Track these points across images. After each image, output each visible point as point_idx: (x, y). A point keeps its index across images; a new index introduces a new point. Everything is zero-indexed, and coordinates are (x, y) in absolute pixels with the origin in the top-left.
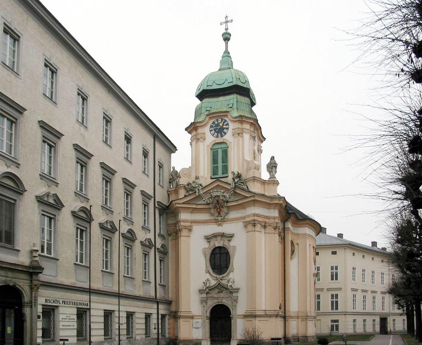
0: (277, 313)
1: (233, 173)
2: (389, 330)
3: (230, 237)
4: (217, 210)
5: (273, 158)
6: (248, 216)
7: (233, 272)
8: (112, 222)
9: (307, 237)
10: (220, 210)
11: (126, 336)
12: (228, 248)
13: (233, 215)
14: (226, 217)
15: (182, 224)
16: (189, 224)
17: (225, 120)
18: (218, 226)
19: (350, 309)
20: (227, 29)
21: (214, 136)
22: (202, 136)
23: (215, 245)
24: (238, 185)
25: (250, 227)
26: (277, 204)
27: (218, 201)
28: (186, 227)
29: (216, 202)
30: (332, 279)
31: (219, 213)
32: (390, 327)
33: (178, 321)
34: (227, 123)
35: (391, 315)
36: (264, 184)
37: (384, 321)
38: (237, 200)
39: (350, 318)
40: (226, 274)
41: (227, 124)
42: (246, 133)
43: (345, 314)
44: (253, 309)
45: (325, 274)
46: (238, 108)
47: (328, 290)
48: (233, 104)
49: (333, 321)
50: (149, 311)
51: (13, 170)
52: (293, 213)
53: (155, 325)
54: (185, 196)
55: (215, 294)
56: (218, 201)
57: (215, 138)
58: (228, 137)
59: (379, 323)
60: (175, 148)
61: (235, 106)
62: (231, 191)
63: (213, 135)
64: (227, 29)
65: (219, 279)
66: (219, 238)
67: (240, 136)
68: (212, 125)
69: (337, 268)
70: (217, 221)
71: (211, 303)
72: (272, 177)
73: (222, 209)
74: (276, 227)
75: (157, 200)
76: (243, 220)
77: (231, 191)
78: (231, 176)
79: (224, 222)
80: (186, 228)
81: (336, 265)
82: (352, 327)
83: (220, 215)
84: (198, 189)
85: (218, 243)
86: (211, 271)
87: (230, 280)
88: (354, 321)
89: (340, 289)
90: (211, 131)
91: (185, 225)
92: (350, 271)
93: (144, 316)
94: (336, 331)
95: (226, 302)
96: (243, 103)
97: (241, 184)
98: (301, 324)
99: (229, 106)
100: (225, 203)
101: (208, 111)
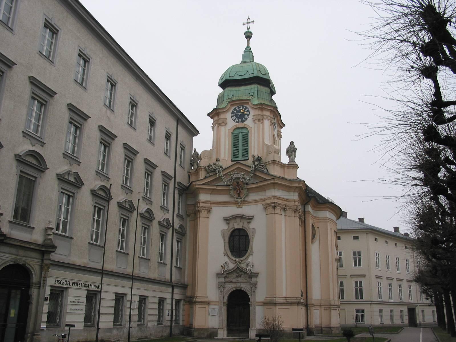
0: (298, 301)
1: (253, 156)
2: (418, 322)
3: (250, 219)
4: (237, 191)
5: (292, 143)
6: (268, 198)
7: (252, 255)
9: (328, 220)
10: (240, 192)
11: (137, 323)
12: (248, 230)
13: (253, 197)
14: (246, 199)
15: (201, 204)
16: (208, 205)
17: (246, 107)
18: (238, 208)
20: (248, 29)
21: (236, 121)
23: (234, 227)
24: (258, 168)
25: (270, 210)
26: (296, 187)
27: (238, 183)
28: (205, 208)
29: (236, 184)
30: (355, 265)
31: (239, 195)
32: (419, 319)
33: (193, 307)
34: (248, 109)
35: (419, 305)
36: (284, 168)
37: (412, 312)
38: (257, 183)
39: (376, 308)
40: (245, 257)
44: (273, 296)
46: (259, 96)
47: (352, 276)
49: (358, 311)
50: (163, 295)
53: (169, 311)
54: (206, 177)
55: (234, 278)
56: (238, 183)
57: (236, 124)
58: (249, 122)
59: (407, 314)
61: (256, 95)
63: (234, 121)
64: (248, 29)
65: (238, 262)
66: (238, 220)
67: (261, 122)
68: (234, 111)
69: (359, 253)
70: (236, 203)
71: (229, 288)
72: (292, 160)
73: (242, 191)
74: (296, 210)
75: (177, 180)
76: (263, 203)
78: (251, 159)
79: (243, 203)
80: (205, 208)
81: (359, 250)
83: (240, 197)
84: (219, 171)
85: (237, 225)
86: (229, 254)
87: (249, 264)
88: (381, 311)
89: (364, 276)
90: (232, 116)
91: (204, 206)
92: (373, 257)
93: (157, 300)
95: (245, 287)
96: (263, 92)
97: (261, 167)
100: (245, 185)
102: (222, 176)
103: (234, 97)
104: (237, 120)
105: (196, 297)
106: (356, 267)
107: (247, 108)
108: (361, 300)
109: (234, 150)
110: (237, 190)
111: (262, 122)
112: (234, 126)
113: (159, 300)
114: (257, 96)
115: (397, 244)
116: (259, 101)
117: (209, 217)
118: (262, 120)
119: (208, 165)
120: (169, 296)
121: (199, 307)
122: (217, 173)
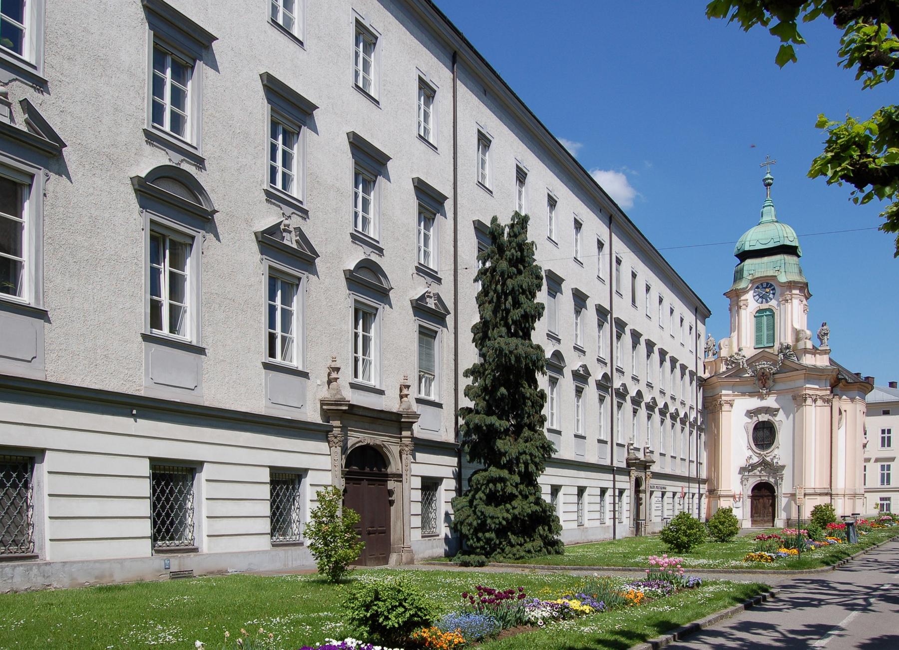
1: (781, 344)
8: (439, 298)
15: (723, 398)
30: (883, 445)
34: (773, 287)
41: (774, 289)
42: (796, 298)
45: (875, 438)
47: (877, 460)
49: (882, 499)
51: (374, 258)
52: (842, 379)
57: (759, 305)
60: (710, 312)
61: (782, 270)
63: (757, 301)
69: (889, 431)
71: (752, 482)
73: (768, 381)
75: (614, 316)
78: (777, 346)
80: (727, 402)
84: (743, 362)
85: (763, 417)
89: (893, 459)
90: (754, 296)
93: (575, 491)
98: (849, 502)
99: (776, 269)
103: (757, 273)
106: (883, 449)
108: (883, 463)
109: (757, 336)
113: (271, 475)
116: (788, 277)
118: (791, 299)
120: (610, 485)
122: (741, 364)
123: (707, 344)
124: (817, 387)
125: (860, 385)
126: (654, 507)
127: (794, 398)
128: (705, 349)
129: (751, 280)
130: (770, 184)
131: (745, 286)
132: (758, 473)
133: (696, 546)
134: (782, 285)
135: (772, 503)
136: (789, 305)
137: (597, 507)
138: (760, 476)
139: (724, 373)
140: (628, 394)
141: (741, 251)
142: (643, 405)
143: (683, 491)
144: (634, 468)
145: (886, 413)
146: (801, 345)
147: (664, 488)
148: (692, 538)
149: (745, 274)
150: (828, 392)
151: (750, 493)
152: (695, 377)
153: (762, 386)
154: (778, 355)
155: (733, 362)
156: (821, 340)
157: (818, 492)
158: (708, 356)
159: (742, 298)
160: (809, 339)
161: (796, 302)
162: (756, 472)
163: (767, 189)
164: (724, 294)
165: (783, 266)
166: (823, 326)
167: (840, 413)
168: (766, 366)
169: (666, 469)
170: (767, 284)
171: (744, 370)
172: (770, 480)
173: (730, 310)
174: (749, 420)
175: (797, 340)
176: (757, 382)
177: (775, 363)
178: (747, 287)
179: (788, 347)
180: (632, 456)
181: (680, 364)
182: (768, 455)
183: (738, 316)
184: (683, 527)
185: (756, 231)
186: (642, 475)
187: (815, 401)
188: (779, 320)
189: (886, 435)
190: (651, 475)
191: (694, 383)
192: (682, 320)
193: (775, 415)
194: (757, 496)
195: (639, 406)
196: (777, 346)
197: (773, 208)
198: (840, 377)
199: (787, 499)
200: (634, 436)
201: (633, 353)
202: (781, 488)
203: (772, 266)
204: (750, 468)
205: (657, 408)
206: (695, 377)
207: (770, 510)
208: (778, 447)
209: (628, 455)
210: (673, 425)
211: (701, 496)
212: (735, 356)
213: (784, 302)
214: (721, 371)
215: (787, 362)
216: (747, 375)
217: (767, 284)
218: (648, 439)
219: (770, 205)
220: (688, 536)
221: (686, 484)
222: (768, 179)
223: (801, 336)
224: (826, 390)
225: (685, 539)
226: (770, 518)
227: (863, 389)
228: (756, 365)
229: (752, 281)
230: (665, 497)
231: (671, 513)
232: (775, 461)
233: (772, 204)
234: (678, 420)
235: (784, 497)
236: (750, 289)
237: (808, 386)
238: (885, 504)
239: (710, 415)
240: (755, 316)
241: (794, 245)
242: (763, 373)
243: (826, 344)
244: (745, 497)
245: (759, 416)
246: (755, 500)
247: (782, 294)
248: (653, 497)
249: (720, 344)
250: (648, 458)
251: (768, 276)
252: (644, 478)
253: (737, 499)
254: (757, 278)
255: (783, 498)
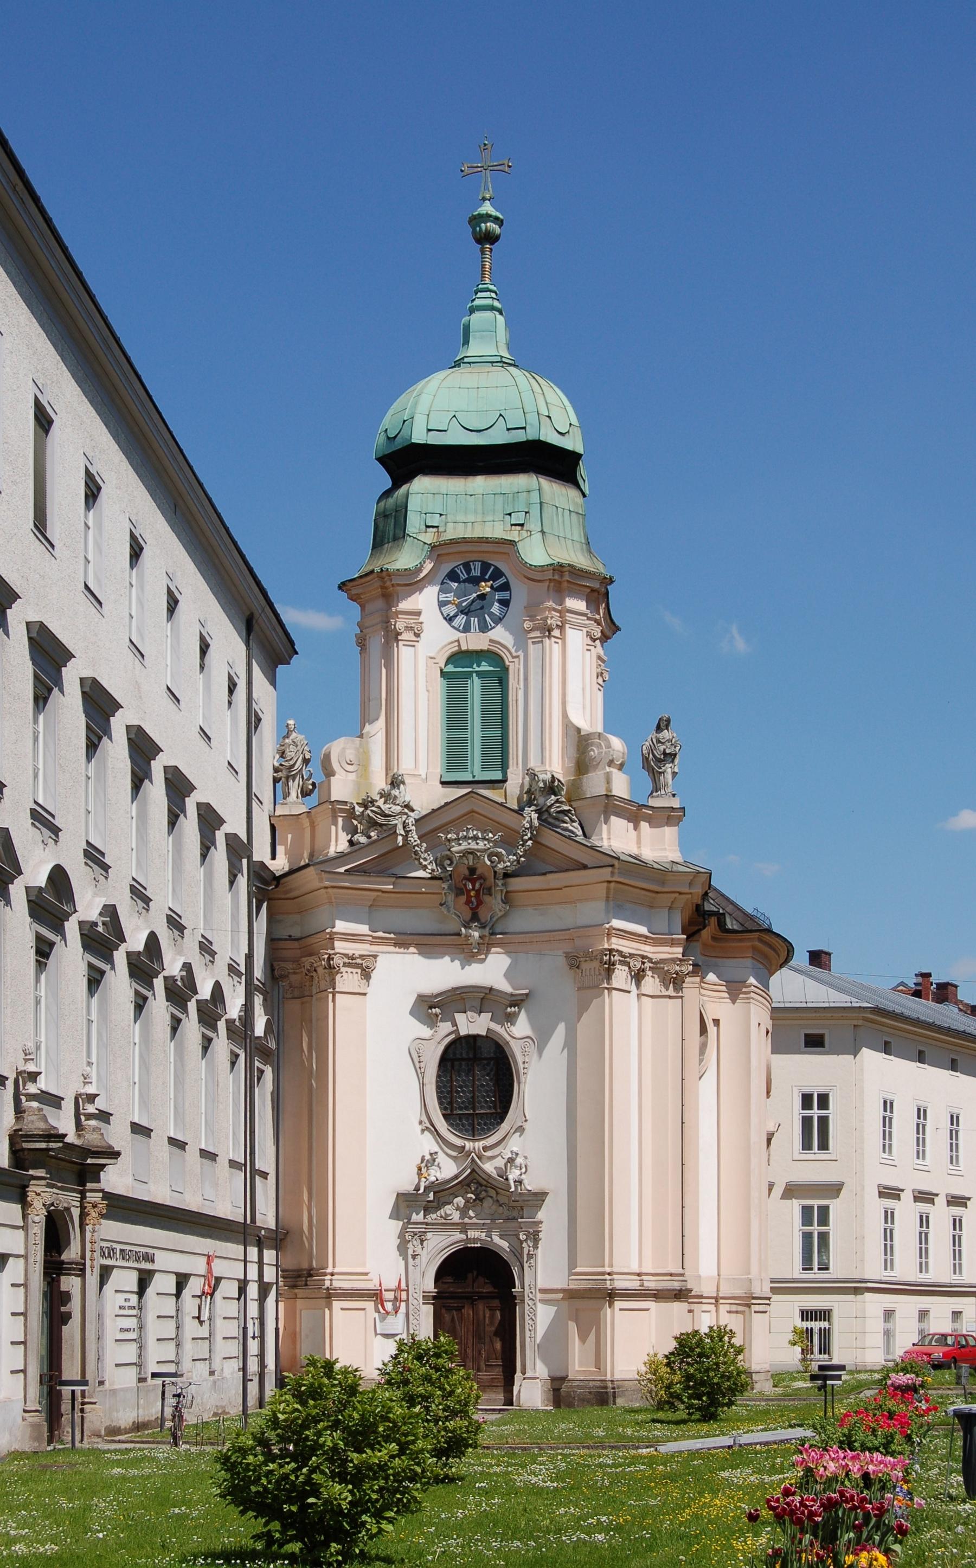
1: (533, 775)
4: (468, 902)
9: (752, 995)
15: (340, 946)
17: (496, 568)
19: (874, 1271)
21: (456, 622)
22: (411, 621)
29: (467, 872)
30: (807, 1145)
39: (875, 1304)
41: (506, 587)
42: (578, 627)
43: (857, 1288)
46: (545, 530)
47: (791, 1191)
48: (526, 513)
49: (807, 1315)
57: (458, 635)
60: (292, 643)
61: (534, 525)
62: (527, 841)
65: (473, 1154)
67: (555, 637)
69: (824, 1101)
73: (486, 898)
77: (526, 838)
78: (516, 781)
80: (352, 962)
81: (823, 1090)
82: (879, 1339)
84: (405, 826)
88: (889, 1314)
89: (834, 1190)
90: (442, 604)
91: (350, 953)
94: (820, 1353)
97: (561, 816)
101: (431, 529)
102: (417, 845)
103: (450, 525)
104: (451, 610)
105: (332, 1274)
107: (491, 565)
110: (469, 897)
111: (563, 638)
112: (446, 646)
114: (540, 530)
115: (923, 1052)
117: (365, 994)
118: (561, 628)
119: (363, 799)
121: (342, 1309)
122: (400, 830)
123: (282, 754)
124: (643, 930)
125: (760, 940)
126: (112, 1328)
127: (574, 962)
128: (276, 770)
129: (433, 547)
130: (488, 239)
131: (411, 565)
132: (456, 1217)
133: (386, 1526)
134: (533, 575)
135: (501, 1323)
136: (553, 648)
137: (132, 1323)
138: (464, 1228)
139: (341, 856)
140: (20, 873)
141: (399, 444)
142: (71, 927)
143: (210, 1270)
144: (41, 1173)
145: (814, 1042)
146: (594, 785)
147: (149, 1258)
148: (372, 1489)
149: (414, 523)
150: (678, 951)
151: (429, 1285)
152: (245, 861)
153: (468, 914)
154: (520, 811)
155: (373, 824)
156: (655, 775)
157: (652, 1285)
158: (286, 795)
159: (404, 605)
160: (621, 767)
161: (576, 638)
162: (452, 1212)
163: (483, 252)
164: (342, 587)
165: (535, 511)
166: (659, 729)
167: (703, 1030)
168: (481, 845)
169: (152, 1186)
170: (485, 566)
171: (407, 853)
172: (496, 1239)
173: (362, 643)
174: (425, 1032)
175: (582, 765)
176: (451, 898)
177: (510, 840)
178: (419, 569)
179: (552, 788)
180: (33, 1124)
181: (199, 805)
182: (489, 1154)
183: (389, 666)
184: (327, 1440)
185: (445, 384)
186: (70, 1200)
187: (638, 977)
188: (521, 693)
189: (815, 1112)
190: (103, 1205)
191: (242, 881)
192: (204, 648)
193: (511, 1019)
194: (453, 1296)
195: (59, 928)
196: (516, 781)
197: (501, 319)
198: (708, 907)
199: (553, 1309)
200: (38, 1048)
201: (36, 721)
202: (534, 1268)
203: (499, 506)
204: (431, 1196)
205: (123, 948)
206: (245, 861)
207: (498, 1345)
208: (521, 1129)
209: (18, 1118)
210: (176, 1024)
211: (264, 1289)
212: (380, 802)
213: (537, 634)
214: (332, 851)
215: (551, 839)
216: (420, 874)
217: (485, 566)
218: (90, 1064)
219: (492, 308)
220: (356, 1478)
221: (236, 1250)
222: (487, 217)
223: (594, 752)
224: (673, 943)
225: (342, 1494)
226: (497, 1373)
227: (766, 956)
228: (449, 840)
229: (438, 550)
230: (150, 1291)
231: (169, 1351)
232: (513, 1175)
233: (496, 304)
234: (192, 1006)
235: (543, 1301)
236: (428, 580)
237: (617, 923)
238: (816, 1331)
239: (293, 1007)
240: (443, 674)
241: (570, 448)
242: (472, 870)
243: (669, 790)
244: (416, 1299)
245: (460, 1018)
246: (449, 1309)
247: (532, 610)
248: (109, 1288)
249: (327, 757)
250: (91, 1139)
251: (485, 541)
252: (76, 1213)
253: (389, 1306)
254: (453, 542)
255: (539, 1306)
